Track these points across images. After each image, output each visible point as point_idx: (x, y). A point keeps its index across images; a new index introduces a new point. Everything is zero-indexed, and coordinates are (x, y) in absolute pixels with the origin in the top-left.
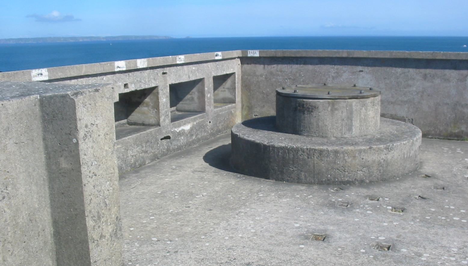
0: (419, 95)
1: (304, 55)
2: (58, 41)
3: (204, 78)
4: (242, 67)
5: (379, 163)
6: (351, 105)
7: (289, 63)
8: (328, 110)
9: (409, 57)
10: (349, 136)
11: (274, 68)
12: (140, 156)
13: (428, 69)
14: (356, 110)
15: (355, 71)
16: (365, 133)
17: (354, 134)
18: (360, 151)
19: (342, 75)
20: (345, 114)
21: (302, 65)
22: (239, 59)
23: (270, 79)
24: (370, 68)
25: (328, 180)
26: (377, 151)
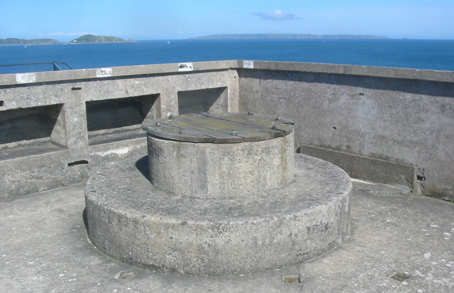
0: (434, 136)
1: (297, 69)
2: (278, 38)
3: (158, 95)
4: (240, 81)
5: (200, 249)
6: (203, 152)
7: (284, 79)
8: (173, 156)
9: (419, 78)
10: (202, 196)
11: (270, 83)
12: (27, 182)
13: (447, 98)
14: (212, 160)
15: (354, 93)
16: (232, 195)
17: (211, 194)
18: (167, 226)
19: (340, 98)
20: (194, 165)
21: (297, 82)
22: (235, 72)
23: (266, 97)
24: (372, 91)
25: (130, 258)
26: (195, 230)
